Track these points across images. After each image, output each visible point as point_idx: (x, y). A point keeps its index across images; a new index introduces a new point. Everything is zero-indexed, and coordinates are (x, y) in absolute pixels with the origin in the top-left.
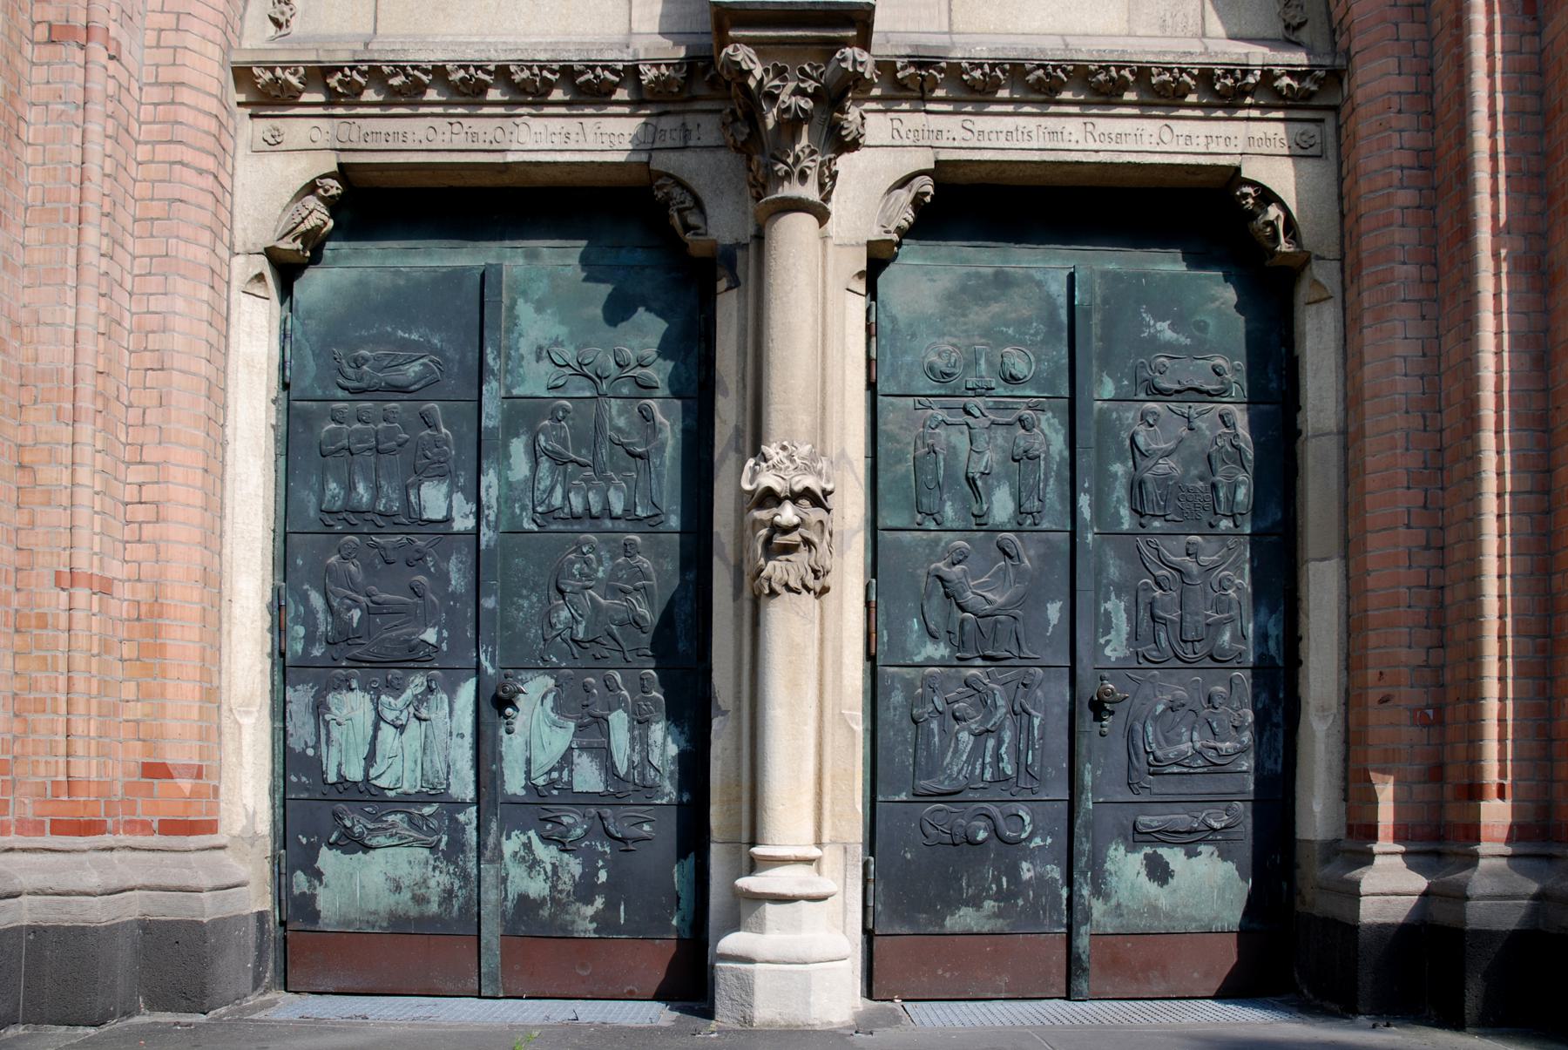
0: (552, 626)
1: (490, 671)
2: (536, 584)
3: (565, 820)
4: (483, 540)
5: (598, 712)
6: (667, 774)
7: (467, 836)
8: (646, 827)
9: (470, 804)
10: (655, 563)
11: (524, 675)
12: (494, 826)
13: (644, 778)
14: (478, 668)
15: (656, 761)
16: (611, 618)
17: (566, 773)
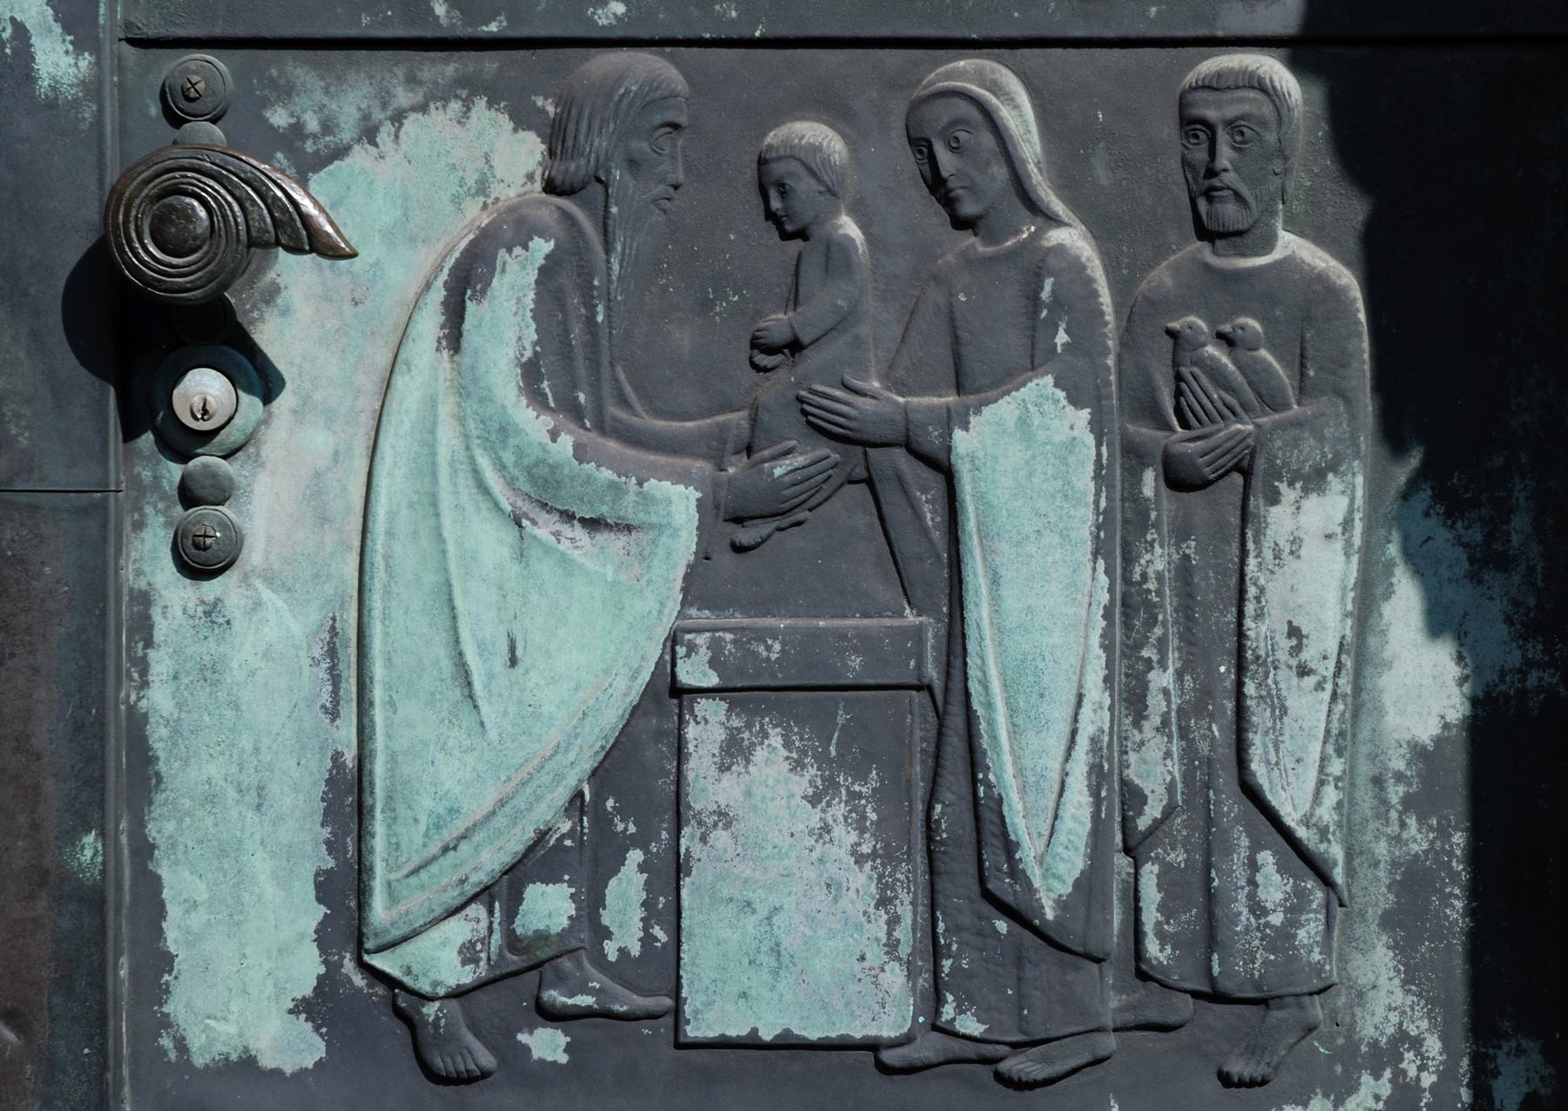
5: (877, 399)
6: (1375, 894)
11: (313, 98)
17: (627, 889)
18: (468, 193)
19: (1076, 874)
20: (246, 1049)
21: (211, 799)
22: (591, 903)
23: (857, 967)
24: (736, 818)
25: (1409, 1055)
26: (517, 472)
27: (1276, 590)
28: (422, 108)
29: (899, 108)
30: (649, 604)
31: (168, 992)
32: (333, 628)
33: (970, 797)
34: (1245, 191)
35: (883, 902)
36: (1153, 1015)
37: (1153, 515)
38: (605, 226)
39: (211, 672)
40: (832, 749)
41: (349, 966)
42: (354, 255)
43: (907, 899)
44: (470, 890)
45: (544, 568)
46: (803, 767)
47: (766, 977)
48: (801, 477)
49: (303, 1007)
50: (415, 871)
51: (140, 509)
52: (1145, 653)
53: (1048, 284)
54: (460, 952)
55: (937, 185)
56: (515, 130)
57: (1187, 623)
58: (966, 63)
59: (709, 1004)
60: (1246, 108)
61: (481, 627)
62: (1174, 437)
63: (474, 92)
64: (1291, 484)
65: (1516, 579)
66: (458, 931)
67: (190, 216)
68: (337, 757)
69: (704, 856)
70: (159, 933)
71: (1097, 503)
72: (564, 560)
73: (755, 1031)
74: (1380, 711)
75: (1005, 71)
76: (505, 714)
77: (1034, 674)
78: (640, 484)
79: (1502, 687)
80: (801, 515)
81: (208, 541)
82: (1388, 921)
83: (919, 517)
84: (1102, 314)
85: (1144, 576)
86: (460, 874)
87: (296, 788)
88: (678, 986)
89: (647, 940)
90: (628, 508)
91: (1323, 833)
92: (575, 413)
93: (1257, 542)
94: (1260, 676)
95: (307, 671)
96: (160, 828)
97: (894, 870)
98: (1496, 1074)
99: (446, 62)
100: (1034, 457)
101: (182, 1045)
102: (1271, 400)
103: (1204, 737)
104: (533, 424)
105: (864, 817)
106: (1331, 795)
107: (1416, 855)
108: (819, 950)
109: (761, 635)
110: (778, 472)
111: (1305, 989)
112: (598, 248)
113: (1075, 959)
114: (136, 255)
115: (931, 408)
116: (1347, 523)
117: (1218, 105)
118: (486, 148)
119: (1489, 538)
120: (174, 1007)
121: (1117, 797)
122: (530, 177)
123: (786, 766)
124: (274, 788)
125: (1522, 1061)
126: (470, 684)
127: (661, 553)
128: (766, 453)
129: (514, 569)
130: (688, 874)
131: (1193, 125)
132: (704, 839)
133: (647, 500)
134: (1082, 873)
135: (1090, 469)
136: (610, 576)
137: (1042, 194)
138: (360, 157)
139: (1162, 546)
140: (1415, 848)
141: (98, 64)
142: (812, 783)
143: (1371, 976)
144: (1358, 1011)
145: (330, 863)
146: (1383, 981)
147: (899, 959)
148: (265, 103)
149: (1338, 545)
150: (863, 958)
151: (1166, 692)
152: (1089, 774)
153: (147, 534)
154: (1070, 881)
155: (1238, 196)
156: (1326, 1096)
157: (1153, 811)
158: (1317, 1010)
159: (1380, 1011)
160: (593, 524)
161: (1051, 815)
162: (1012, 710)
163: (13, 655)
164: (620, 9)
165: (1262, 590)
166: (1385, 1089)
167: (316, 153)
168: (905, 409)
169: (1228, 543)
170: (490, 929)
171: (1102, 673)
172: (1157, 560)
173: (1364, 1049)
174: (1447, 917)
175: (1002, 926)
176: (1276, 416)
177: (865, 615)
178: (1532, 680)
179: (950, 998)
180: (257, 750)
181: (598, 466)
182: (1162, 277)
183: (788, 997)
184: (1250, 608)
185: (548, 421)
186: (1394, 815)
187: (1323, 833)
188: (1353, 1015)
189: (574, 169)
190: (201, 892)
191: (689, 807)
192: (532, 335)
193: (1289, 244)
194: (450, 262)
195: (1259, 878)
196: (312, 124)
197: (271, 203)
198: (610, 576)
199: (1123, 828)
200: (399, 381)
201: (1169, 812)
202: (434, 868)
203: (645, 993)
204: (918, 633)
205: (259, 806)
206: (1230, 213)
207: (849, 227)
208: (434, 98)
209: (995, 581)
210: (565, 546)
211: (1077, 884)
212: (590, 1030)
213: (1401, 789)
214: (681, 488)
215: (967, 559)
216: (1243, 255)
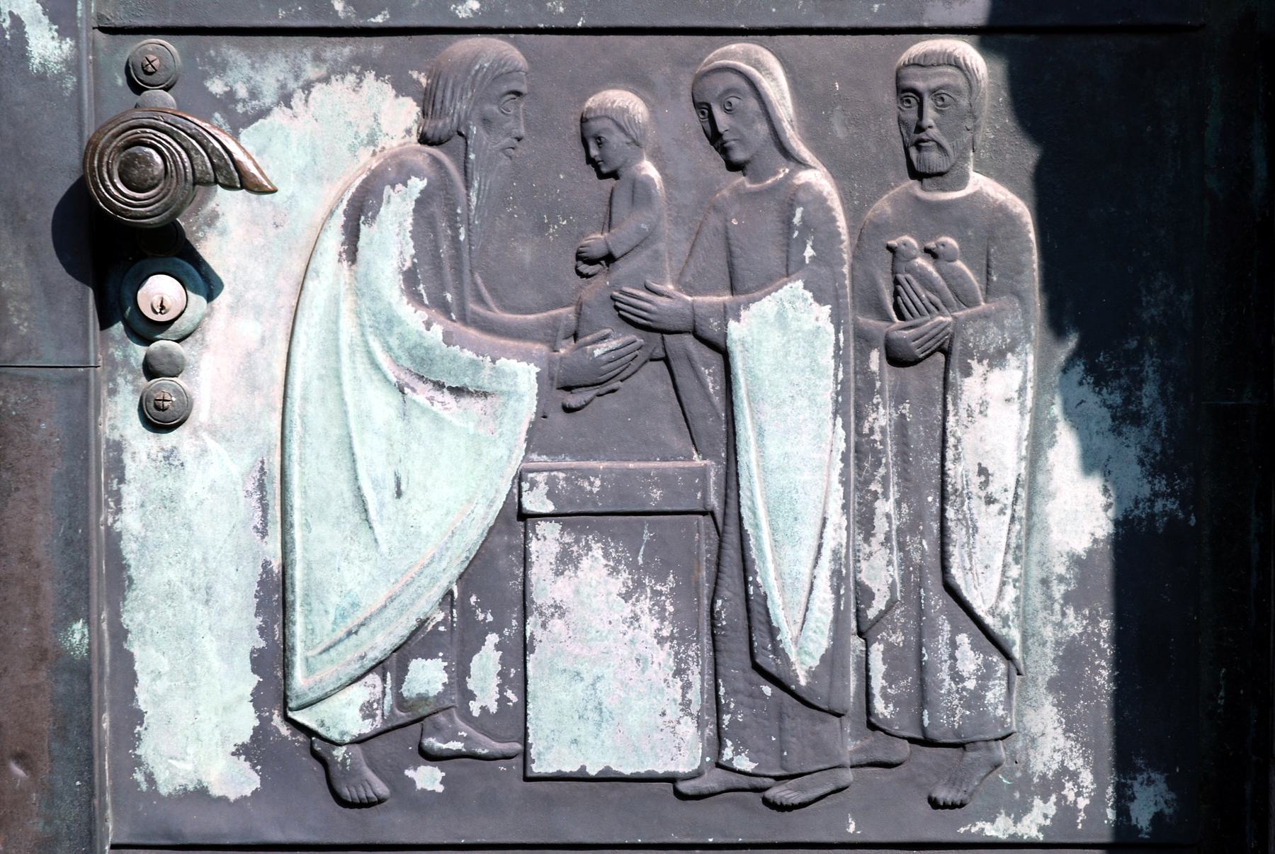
5: (671, 298)
6: (1044, 665)
13: (923, 694)
17: (486, 664)
18: (361, 143)
19: (823, 651)
20: (200, 782)
22: (460, 673)
23: (660, 720)
26: (400, 353)
27: (969, 440)
28: (326, 80)
29: (686, 81)
31: (139, 739)
32: (262, 469)
34: (944, 142)
35: (679, 672)
36: (880, 756)
37: (878, 384)
38: (465, 168)
39: (170, 502)
41: (277, 720)
42: (274, 191)
43: (696, 670)
44: (368, 664)
45: (422, 424)
46: (618, 572)
47: (591, 727)
48: (615, 356)
49: (243, 751)
50: (327, 650)
51: (114, 380)
52: (873, 487)
53: (799, 212)
54: (361, 710)
55: (715, 137)
56: (397, 96)
57: (904, 469)
58: (737, 46)
59: (549, 748)
60: (946, 80)
61: (374, 466)
63: (365, 68)
64: (980, 361)
65: (1147, 431)
67: (149, 162)
71: (836, 375)
72: (437, 419)
73: (583, 768)
74: (1046, 530)
75: (766, 52)
76: (393, 532)
78: (493, 361)
79: (1137, 512)
80: (615, 384)
82: (1053, 686)
83: (703, 386)
84: (839, 234)
85: (872, 430)
86: (361, 652)
87: (235, 588)
89: (502, 700)
90: (485, 380)
91: (1005, 621)
92: (445, 308)
93: (955, 404)
95: (242, 500)
96: (132, 618)
97: (687, 649)
100: (789, 341)
101: (150, 779)
102: (965, 300)
103: (917, 549)
104: (412, 317)
105: (664, 609)
106: (1011, 593)
107: (1074, 637)
108: (631, 708)
109: (585, 474)
110: (597, 352)
111: (992, 736)
114: (108, 191)
115: (711, 305)
116: (1022, 391)
117: (925, 78)
118: (375, 110)
119: (1127, 401)
120: (144, 751)
122: (408, 132)
123: (605, 571)
124: (219, 588)
125: (1152, 789)
126: (366, 511)
127: (510, 412)
128: (589, 338)
129: (399, 425)
131: (905, 93)
132: (544, 626)
133: (498, 374)
134: (827, 650)
135: (831, 350)
138: (279, 116)
139: (884, 408)
140: (1073, 631)
141: (77, 46)
143: (1041, 727)
144: (1031, 752)
146: (1049, 730)
148: (206, 76)
149: (1015, 407)
150: (664, 714)
151: (888, 516)
152: (832, 577)
154: (818, 656)
156: (1008, 815)
157: (879, 604)
158: (1001, 751)
159: (1048, 752)
160: (458, 391)
161: (803, 607)
162: (774, 530)
163: (17, 489)
165: (959, 440)
166: (1051, 809)
167: (245, 113)
168: (692, 306)
171: (841, 502)
172: (881, 418)
173: (1036, 780)
174: (1096, 683)
175: (767, 690)
176: (969, 311)
177: (664, 459)
179: (729, 743)
180: (205, 560)
181: (462, 348)
182: (883, 206)
183: (608, 743)
184: (950, 454)
185: (423, 314)
186: (1057, 607)
187: (1005, 621)
189: (441, 126)
191: (533, 602)
193: (978, 183)
194: (348, 196)
195: (958, 654)
196: (242, 92)
198: (471, 431)
201: (891, 605)
202: (340, 648)
204: (703, 473)
205: (207, 601)
206: (933, 159)
207: (649, 169)
209: (760, 434)
210: (437, 408)
211: (823, 658)
213: (1063, 588)
214: (524, 364)
216: (944, 190)
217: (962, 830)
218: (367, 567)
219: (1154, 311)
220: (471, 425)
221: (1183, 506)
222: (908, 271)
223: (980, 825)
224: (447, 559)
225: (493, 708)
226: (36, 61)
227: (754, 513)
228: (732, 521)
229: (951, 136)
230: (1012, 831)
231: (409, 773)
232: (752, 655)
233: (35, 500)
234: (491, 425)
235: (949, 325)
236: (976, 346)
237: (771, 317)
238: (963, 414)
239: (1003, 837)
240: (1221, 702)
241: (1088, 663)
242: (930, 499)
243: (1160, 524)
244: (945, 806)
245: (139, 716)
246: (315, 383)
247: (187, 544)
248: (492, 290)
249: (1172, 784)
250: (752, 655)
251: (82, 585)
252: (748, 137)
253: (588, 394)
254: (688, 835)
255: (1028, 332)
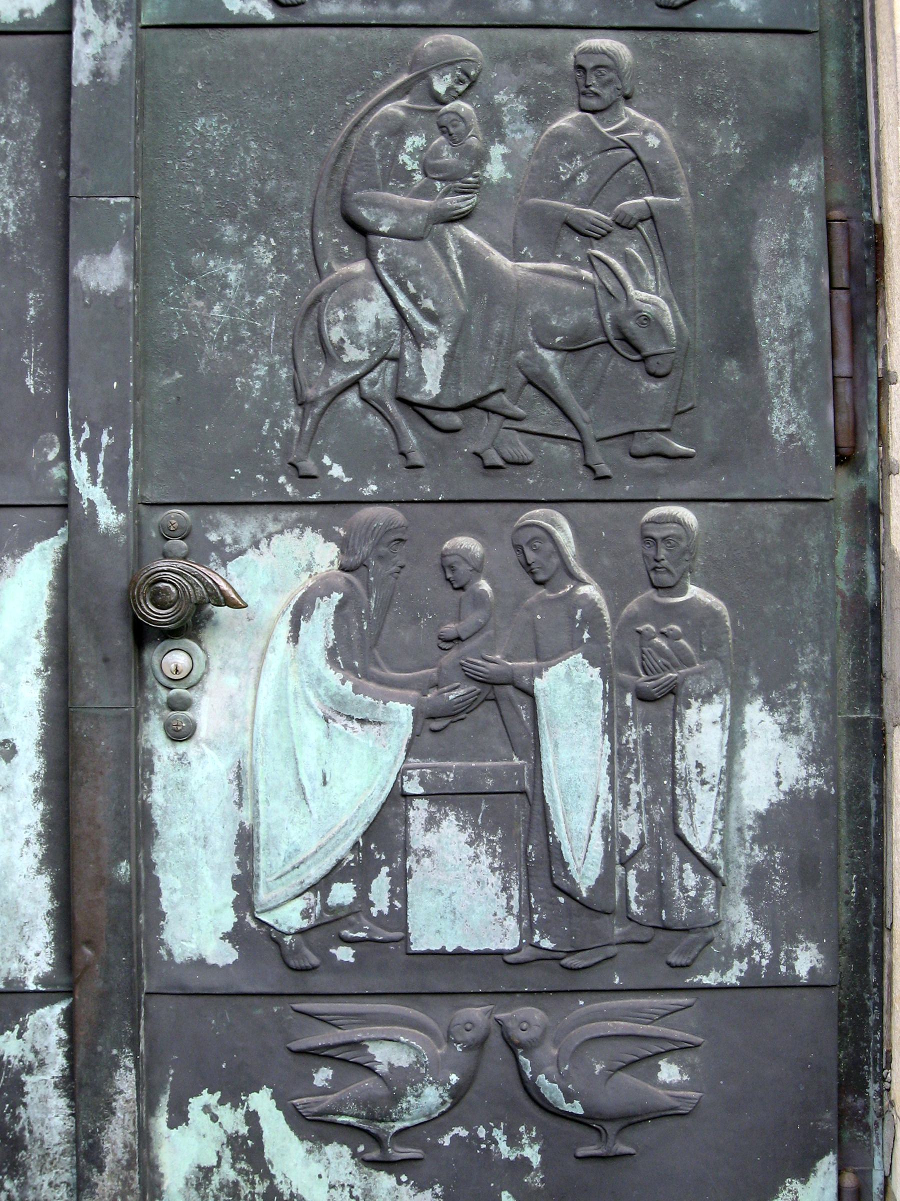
0: (329, 354)
1: (108, 517)
2: (269, 203)
3: (386, 1055)
4: (84, 53)
5: (498, 662)
6: (739, 879)
7: (30, 1112)
8: (669, 1072)
9: (44, 997)
10: (685, 132)
11: (227, 528)
12: (125, 1083)
13: (663, 899)
14: (65, 506)
15: (701, 834)
16: (539, 322)
17: (380, 889)
18: (303, 570)
19: (597, 876)
20: (200, 955)
21: (182, 842)
22: (363, 891)
23: (493, 918)
24: (433, 852)
25: (756, 952)
26: (325, 698)
27: (690, 747)
28: (281, 532)
29: (508, 532)
30: (390, 758)
31: (163, 929)
32: (239, 766)
33: (545, 842)
34: (671, 568)
35: (505, 889)
36: (634, 937)
37: (631, 714)
38: (368, 586)
39: (181, 786)
40: (479, 821)
41: (248, 918)
42: (247, 606)
43: (516, 887)
44: (305, 886)
45: (340, 741)
46: (466, 829)
47: (448, 923)
48: (462, 699)
49: (226, 936)
50: (279, 877)
51: (147, 712)
52: (629, 776)
53: (579, 612)
54: (301, 914)
55: (527, 567)
56: (325, 542)
57: (648, 763)
58: (539, 511)
59: (421, 936)
60: (672, 531)
61: (310, 766)
62: (640, 679)
63: (306, 525)
64: (696, 700)
65: (803, 738)
66: (300, 904)
67: (166, 591)
68: (241, 824)
69: (418, 870)
70: (159, 903)
71: (604, 709)
72: (349, 738)
73: (444, 947)
74: (741, 799)
75: (558, 514)
76: (321, 806)
77: (576, 787)
78: (385, 703)
79: (797, 786)
80: (462, 716)
81: (179, 728)
82: (745, 892)
83: (520, 716)
84: (606, 624)
85: (628, 742)
86: (301, 879)
87: (222, 838)
88: (407, 928)
89: (392, 907)
90: (379, 715)
91: (714, 855)
92: (354, 671)
93: (681, 725)
94: (683, 786)
95: (227, 785)
96: (158, 855)
97: (510, 874)
98: (796, 959)
99: (292, 511)
100: (573, 690)
101: (170, 953)
102: (688, 663)
103: (657, 813)
104: (333, 677)
105: (495, 851)
106: (718, 838)
107: (758, 862)
108: (474, 911)
109: (444, 770)
110: (451, 697)
111: (706, 924)
112: (365, 596)
113: (597, 914)
114: (143, 610)
115: (524, 668)
116: (723, 717)
117: (659, 530)
118: (311, 550)
119: (790, 720)
120: (166, 936)
121: (611, 834)
122: (332, 563)
123: (457, 828)
124: (212, 838)
125: (808, 953)
126: (304, 794)
127: (395, 733)
128: (445, 688)
129: (326, 741)
130: (411, 877)
131: (647, 539)
132: (418, 862)
133: (388, 711)
134: (600, 875)
135: (600, 695)
136: (371, 745)
137: (576, 571)
138: (251, 554)
139: (636, 728)
140: (758, 859)
141: (127, 518)
142: (470, 836)
143: (738, 917)
144: (732, 932)
145: (239, 872)
146: (743, 919)
147: (512, 914)
148: (206, 531)
149: (719, 726)
150: (495, 914)
151: (639, 794)
152: (602, 831)
153: (151, 723)
154: (594, 879)
155: (668, 571)
156: (717, 971)
157: (633, 846)
158: (713, 933)
159: (742, 932)
160: (362, 721)
161: (584, 850)
162: (565, 803)
163: (87, 781)
164: (375, 488)
165: (683, 747)
166: (745, 967)
167: (231, 553)
168: (512, 669)
169: (667, 725)
170: (316, 903)
171: (608, 786)
172: (632, 734)
173: (735, 949)
174: (773, 890)
175: (562, 900)
176: (688, 670)
177: (494, 760)
178: (811, 783)
179: (537, 932)
180: (203, 821)
181: (364, 696)
182: (633, 606)
183: (459, 932)
184: (678, 755)
185: (340, 675)
186: (748, 845)
187: (714, 855)
188: (730, 934)
189: (354, 560)
190: (179, 886)
191: (411, 847)
192: (332, 636)
193: (694, 591)
194: (293, 603)
195: (684, 875)
196: (229, 540)
197: (207, 586)
198: (371, 745)
199: (616, 854)
200: (269, 656)
201: (641, 847)
202: (288, 876)
203: (391, 931)
204: (520, 769)
205: (205, 846)
206: (666, 579)
207: (484, 585)
208: (287, 528)
209: (556, 745)
210: (349, 731)
211: (597, 881)
212: (363, 947)
213: (751, 833)
214: (405, 705)
215: (542, 735)
216: (671, 597)
217: (688, 980)
218: (305, 827)
219: (806, 666)
220: (371, 743)
221: (826, 782)
222: (649, 646)
223: (699, 977)
224: (355, 823)
225: (386, 911)
226: (102, 527)
227: (552, 794)
228: (538, 798)
229: (676, 564)
230: (719, 980)
231: (332, 951)
232: (552, 879)
233: (97, 788)
234: (384, 742)
235: (676, 678)
236: (693, 691)
237: (562, 675)
238: (686, 731)
239: (713, 984)
240: (854, 895)
241: (768, 878)
242: (665, 782)
243: (812, 794)
244: (676, 966)
245: (163, 915)
246: (272, 715)
247: (192, 811)
248: (383, 658)
249: (821, 949)
250: (552, 879)
251: (125, 839)
252: (547, 567)
253: (445, 722)
254: (511, 987)
255: (726, 681)
